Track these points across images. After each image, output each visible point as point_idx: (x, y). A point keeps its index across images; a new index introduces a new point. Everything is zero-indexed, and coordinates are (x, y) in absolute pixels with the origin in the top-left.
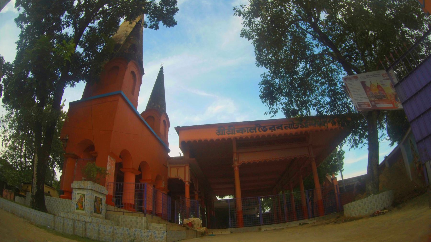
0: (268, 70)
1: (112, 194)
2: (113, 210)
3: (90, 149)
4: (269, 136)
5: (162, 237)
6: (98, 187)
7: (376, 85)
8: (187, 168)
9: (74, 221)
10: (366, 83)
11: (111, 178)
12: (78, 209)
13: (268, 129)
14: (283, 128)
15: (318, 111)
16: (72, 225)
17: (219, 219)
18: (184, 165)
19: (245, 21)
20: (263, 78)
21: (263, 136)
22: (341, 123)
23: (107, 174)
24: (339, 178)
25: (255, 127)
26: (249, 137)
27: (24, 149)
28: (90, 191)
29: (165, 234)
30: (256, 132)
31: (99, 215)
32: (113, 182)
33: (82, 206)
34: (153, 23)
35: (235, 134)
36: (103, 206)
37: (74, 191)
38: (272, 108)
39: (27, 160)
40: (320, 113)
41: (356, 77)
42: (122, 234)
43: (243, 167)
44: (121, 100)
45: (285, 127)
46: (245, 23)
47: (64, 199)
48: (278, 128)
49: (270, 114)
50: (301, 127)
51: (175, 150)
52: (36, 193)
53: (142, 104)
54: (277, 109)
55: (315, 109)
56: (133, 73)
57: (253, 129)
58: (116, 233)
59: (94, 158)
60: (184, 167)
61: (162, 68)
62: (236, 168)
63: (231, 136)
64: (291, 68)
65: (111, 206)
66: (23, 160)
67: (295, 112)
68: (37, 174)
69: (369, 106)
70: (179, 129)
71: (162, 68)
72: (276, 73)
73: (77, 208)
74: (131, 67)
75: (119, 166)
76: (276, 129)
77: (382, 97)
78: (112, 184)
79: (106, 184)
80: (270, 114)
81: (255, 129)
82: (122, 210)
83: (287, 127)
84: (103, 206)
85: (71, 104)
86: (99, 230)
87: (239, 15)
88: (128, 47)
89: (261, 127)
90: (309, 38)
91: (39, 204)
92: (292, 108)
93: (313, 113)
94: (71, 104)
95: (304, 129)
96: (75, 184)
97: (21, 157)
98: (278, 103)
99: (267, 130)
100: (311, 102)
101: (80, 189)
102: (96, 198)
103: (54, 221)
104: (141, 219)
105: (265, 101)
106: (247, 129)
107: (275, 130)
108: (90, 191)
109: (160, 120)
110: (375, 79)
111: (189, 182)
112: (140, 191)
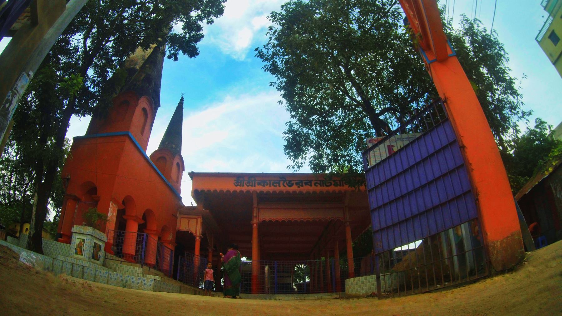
1: (111, 242)
2: (111, 258)
3: (92, 191)
4: (295, 192)
6: (98, 233)
8: (200, 221)
9: (73, 265)
13: (295, 185)
14: (313, 185)
17: (241, 285)
18: (196, 217)
23: (107, 221)
25: (280, 181)
27: (14, 178)
29: (153, 282)
30: (279, 186)
32: (114, 229)
33: (81, 251)
35: (255, 186)
36: (102, 253)
37: (74, 235)
39: (17, 192)
43: (263, 225)
44: (128, 142)
47: (62, 244)
48: (306, 184)
50: (334, 185)
51: (188, 199)
52: (34, 234)
53: (153, 145)
54: (302, 163)
56: (144, 109)
58: (111, 278)
59: (95, 203)
61: (182, 99)
62: (255, 225)
63: (251, 189)
65: (109, 255)
66: (12, 192)
67: (324, 168)
70: (193, 175)
71: (182, 99)
72: (305, 122)
73: (76, 253)
74: (143, 103)
75: (121, 214)
78: (113, 232)
82: (120, 259)
84: (102, 253)
85: (75, 139)
86: (95, 274)
88: (142, 78)
89: (285, 181)
91: (35, 245)
96: (75, 229)
97: (10, 188)
99: (293, 184)
101: (80, 233)
102: (95, 244)
104: (138, 269)
106: (270, 183)
107: (302, 186)
108: (89, 237)
109: (173, 163)
111: (200, 237)
112: (141, 241)
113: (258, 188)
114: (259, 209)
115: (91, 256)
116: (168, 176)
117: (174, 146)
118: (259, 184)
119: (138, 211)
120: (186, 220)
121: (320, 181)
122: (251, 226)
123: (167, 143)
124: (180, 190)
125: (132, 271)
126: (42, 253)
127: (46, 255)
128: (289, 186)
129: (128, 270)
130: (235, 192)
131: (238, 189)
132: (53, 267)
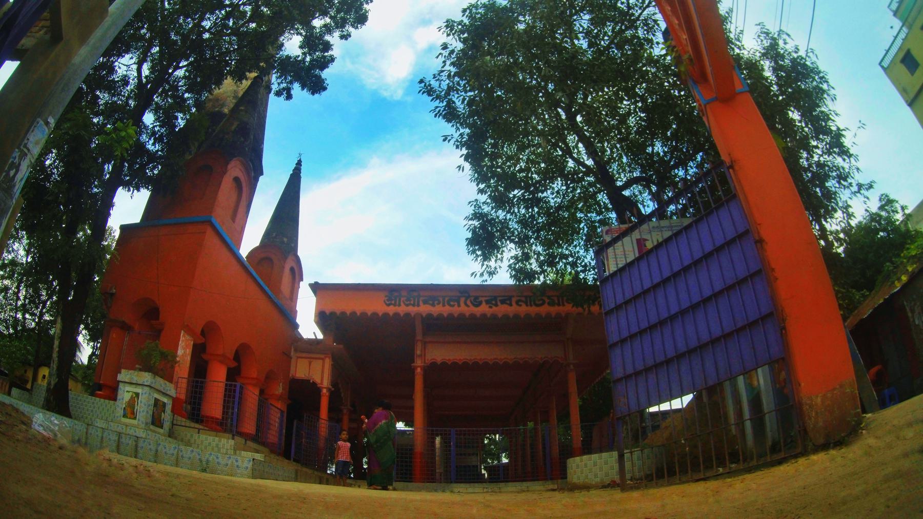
1: (183, 397)
2: (183, 424)
3: (151, 314)
4: (484, 315)
5: (247, 468)
6: (160, 383)
8: (328, 362)
9: (119, 434)
13: (484, 303)
14: (514, 303)
17: (396, 468)
18: (322, 356)
21: (473, 316)
23: (176, 362)
25: (459, 297)
26: (456, 315)
27: (23, 293)
29: (251, 463)
30: (459, 306)
31: (161, 431)
32: (186, 376)
33: (133, 413)
35: (418, 305)
36: (167, 416)
37: (121, 386)
39: (27, 316)
43: (432, 369)
44: (210, 233)
47: (102, 400)
48: (503, 302)
51: (308, 327)
52: (56, 385)
53: (251, 238)
54: (496, 268)
56: (237, 180)
59: (157, 333)
61: (299, 163)
62: (419, 370)
63: (412, 310)
65: (179, 418)
66: (19, 316)
67: (531, 275)
68: (59, 352)
70: (316, 288)
71: (299, 163)
74: (235, 169)
75: (199, 351)
78: (185, 381)
79: (175, 377)
82: (197, 426)
84: (167, 416)
85: (124, 228)
88: (233, 128)
91: (58, 402)
94: (124, 228)
96: (124, 375)
97: (17, 309)
99: (481, 303)
101: (131, 383)
102: (156, 400)
104: (226, 443)
105: (474, 252)
107: (496, 305)
108: (147, 389)
109: (284, 267)
112: (232, 395)
113: (424, 309)
114: (425, 344)
115: (150, 420)
116: (277, 290)
117: (285, 240)
119: (227, 347)
120: (306, 361)
121: (526, 297)
122: (413, 371)
124: (296, 312)
125: (217, 445)
126: (69, 415)
129: (210, 443)
130: (386, 315)
131: (391, 310)
132: (87, 438)
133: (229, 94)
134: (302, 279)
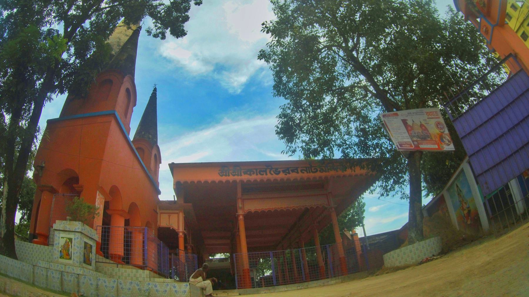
0: (289, 101)
4: (282, 180)
6: (87, 229)
7: (419, 124)
8: (181, 216)
10: (408, 122)
11: (99, 221)
12: (63, 258)
13: (281, 172)
14: (299, 171)
15: (343, 152)
16: (58, 278)
17: (224, 278)
18: (178, 211)
19: (273, 41)
20: (282, 110)
22: (370, 166)
24: (359, 232)
28: (79, 234)
30: (266, 174)
33: (68, 254)
34: (158, 31)
35: (241, 175)
36: (93, 256)
38: (290, 147)
40: (346, 155)
41: (397, 114)
42: (130, 289)
43: (249, 216)
45: (301, 171)
46: (273, 42)
47: (39, 246)
48: (293, 171)
49: (287, 153)
50: (320, 171)
51: (167, 193)
55: (341, 150)
57: (263, 171)
58: (122, 288)
60: (177, 213)
61: (155, 90)
62: (241, 217)
63: (238, 178)
64: (315, 99)
68: (6, 208)
69: (411, 146)
70: (173, 167)
71: (155, 90)
73: (61, 257)
76: (291, 172)
77: (425, 137)
80: (287, 153)
81: (266, 171)
83: (304, 170)
84: (93, 256)
86: (97, 285)
87: (267, 32)
88: (124, 57)
89: (272, 168)
90: (339, 68)
92: (313, 147)
93: (338, 155)
95: (323, 175)
96: (58, 225)
98: (297, 141)
99: (280, 172)
100: (335, 141)
103: (33, 272)
105: (282, 138)
106: (257, 171)
107: (289, 173)
108: (78, 235)
109: (151, 153)
110: (416, 117)
113: (245, 177)
114: (243, 200)
115: (82, 260)
116: (149, 167)
117: (150, 136)
118: (245, 173)
119: (125, 205)
120: (166, 216)
121: (306, 168)
122: (236, 218)
123: (143, 133)
124: (159, 183)
125: (135, 276)
126: (16, 258)
127: (20, 260)
128: (276, 174)
129: (129, 275)
130: (220, 182)
131: (224, 179)
132: (34, 276)
133: (115, 43)
134: (161, 163)
